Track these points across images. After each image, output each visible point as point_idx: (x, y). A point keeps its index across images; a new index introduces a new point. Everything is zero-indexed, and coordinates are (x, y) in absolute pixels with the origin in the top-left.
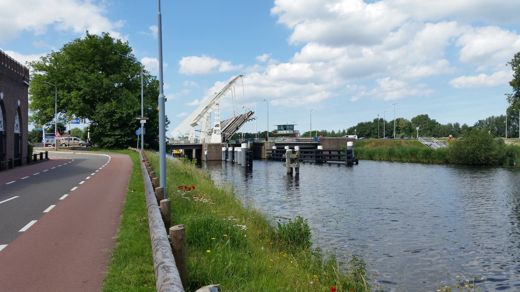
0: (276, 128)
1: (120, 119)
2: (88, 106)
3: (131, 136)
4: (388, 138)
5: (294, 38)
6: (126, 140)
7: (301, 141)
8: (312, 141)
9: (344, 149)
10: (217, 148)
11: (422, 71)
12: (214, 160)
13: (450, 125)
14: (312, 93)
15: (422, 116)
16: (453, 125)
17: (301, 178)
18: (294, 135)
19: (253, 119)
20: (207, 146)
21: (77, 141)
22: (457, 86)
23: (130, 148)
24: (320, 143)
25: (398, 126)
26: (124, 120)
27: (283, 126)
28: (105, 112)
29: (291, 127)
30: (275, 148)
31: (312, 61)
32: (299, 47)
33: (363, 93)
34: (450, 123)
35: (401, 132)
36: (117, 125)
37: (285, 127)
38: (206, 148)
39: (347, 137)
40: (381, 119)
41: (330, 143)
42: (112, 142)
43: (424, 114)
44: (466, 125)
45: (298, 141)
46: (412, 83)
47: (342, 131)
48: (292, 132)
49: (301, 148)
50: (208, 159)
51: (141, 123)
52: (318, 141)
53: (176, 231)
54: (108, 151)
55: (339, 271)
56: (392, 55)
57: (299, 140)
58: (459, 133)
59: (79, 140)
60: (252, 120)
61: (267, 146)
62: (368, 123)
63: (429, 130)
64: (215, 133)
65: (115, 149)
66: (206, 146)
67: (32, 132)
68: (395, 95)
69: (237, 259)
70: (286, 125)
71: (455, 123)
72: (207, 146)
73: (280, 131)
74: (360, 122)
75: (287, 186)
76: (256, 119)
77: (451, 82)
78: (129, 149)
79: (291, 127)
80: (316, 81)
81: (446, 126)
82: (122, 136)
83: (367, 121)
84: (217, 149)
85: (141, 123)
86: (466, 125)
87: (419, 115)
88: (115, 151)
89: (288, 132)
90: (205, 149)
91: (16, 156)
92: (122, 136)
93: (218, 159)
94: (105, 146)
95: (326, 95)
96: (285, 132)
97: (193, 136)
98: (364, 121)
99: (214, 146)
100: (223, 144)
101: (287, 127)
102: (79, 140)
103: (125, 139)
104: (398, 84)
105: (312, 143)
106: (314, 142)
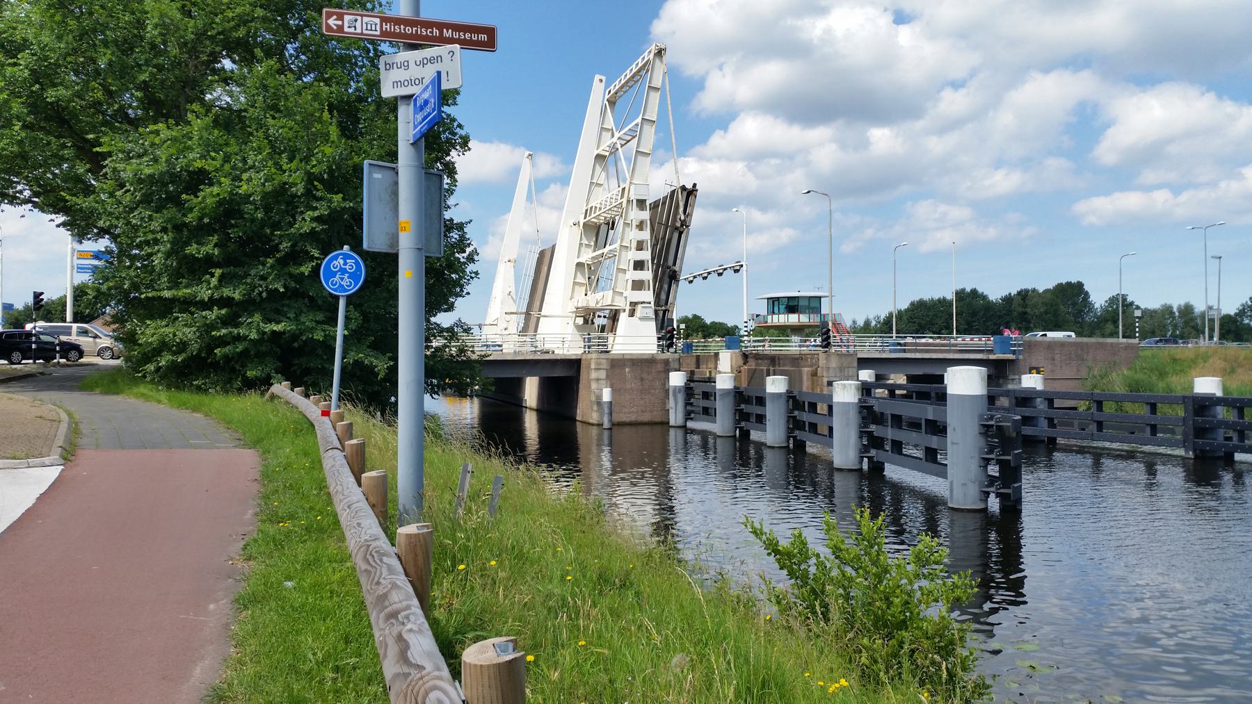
0: (762, 309)
1: (230, 209)
2: (64, 146)
3: (292, 315)
4: (1158, 342)
5: (708, 101)
6: (254, 335)
7: (910, 351)
9: (1227, 394)
10: (645, 376)
11: (1003, 182)
12: (631, 424)
13: (1168, 310)
14: (753, 230)
15: (1069, 284)
16: (1175, 310)
18: (824, 332)
19: (695, 277)
20: (604, 367)
21: (91, 339)
22: (1092, 219)
23: (281, 388)
25: (1023, 310)
26: (253, 220)
28: (148, 171)
29: (813, 304)
30: (870, 376)
31: (755, 157)
32: (723, 120)
33: (869, 233)
34: (1168, 303)
35: (1031, 325)
36: (209, 248)
37: (792, 305)
38: (603, 374)
39: (1042, 335)
40: (957, 293)
41: (1053, 359)
42: (183, 346)
43: (1074, 280)
45: (900, 351)
46: (987, 210)
47: (861, 323)
48: (815, 319)
49: (911, 379)
50: (617, 418)
51: (387, 92)
52: (1014, 352)
53: (409, 536)
54: (163, 395)
56: (937, 146)
57: (905, 345)
58: (1194, 332)
59: (96, 337)
61: (828, 369)
62: (939, 300)
63: (1110, 323)
64: (632, 314)
65: (199, 388)
66: (600, 364)
67: (24, 311)
68: (946, 238)
71: (1183, 303)
73: (775, 317)
74: (917, 298)
77: (1081, 207)
78: (273, 397)
79: (814, 304)
80: (762, 202)
81: (1155, 311)
82: (235, 311)
83: (936, 297)
84: (642, 379)
85: (387, 92)
87: (1062, 284)
88: (195, 398)
89: (804, 319)
90: (598, 380)
92: (235, 311)
93: (658, 419)
94: (151, 367)
95: (786, 235)
96: (793, 319)
97: (510, 328)
98: (927, 296)
99: (633, 365)
100: (668, 360)
101: (802, 303)
102: (96, 337)
103: (253, 327)
104: (958, 213)
105: (992, 357)
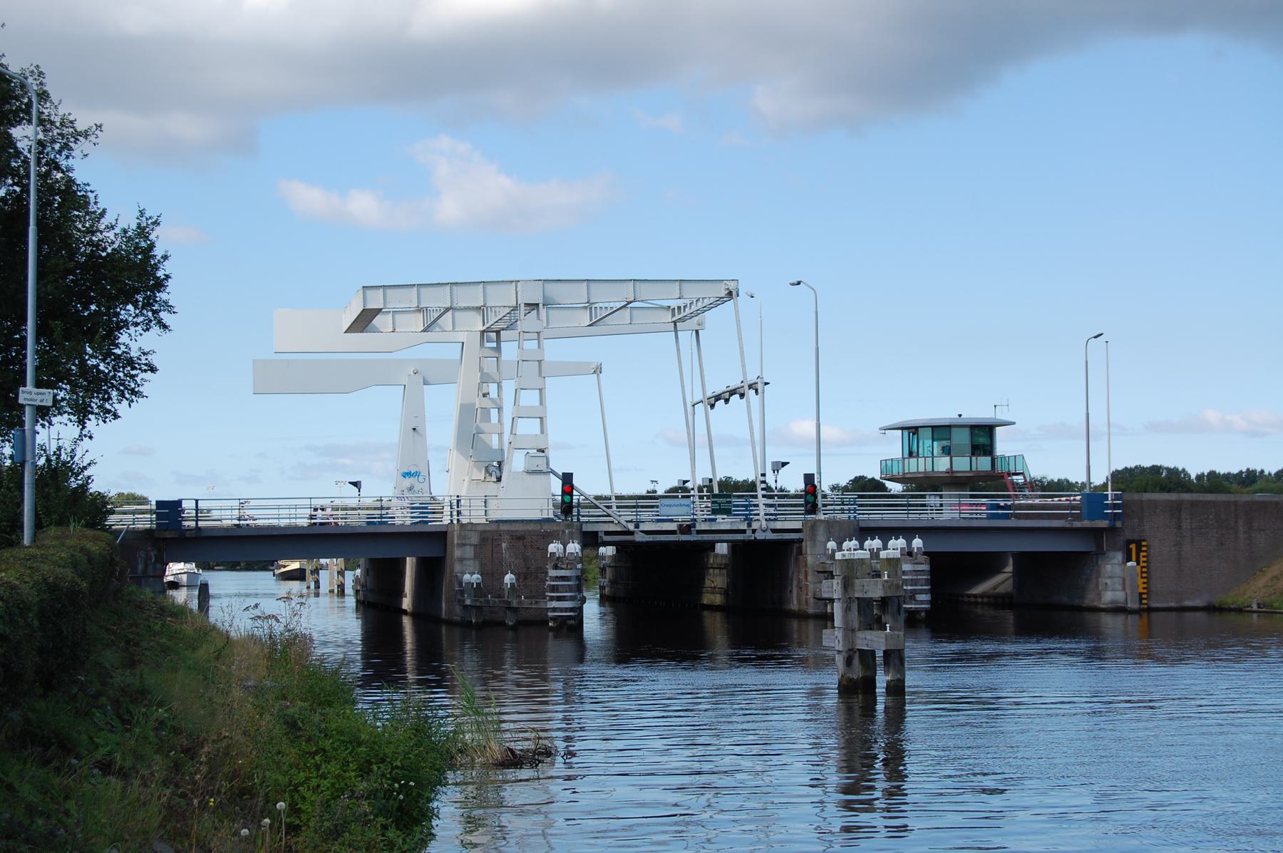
8: (1078, 517)
17: (589, 643)
24: (1119, 524)
27: (935, 428)
38: (469, 552)
44: (1251, 469)
48: (983, 463)
49: (158, 518)
55: (480, 829)
60: (727, 401)
69: (40, 104)
70: (949, 427)
72: (475, 539)
75: (836, 787)
76: (760, 387)
86: (1251, 469)
91: (564, 493)
105: (1077, 524)
106: (1086, 523)
